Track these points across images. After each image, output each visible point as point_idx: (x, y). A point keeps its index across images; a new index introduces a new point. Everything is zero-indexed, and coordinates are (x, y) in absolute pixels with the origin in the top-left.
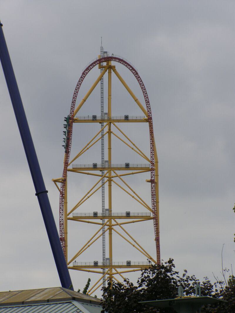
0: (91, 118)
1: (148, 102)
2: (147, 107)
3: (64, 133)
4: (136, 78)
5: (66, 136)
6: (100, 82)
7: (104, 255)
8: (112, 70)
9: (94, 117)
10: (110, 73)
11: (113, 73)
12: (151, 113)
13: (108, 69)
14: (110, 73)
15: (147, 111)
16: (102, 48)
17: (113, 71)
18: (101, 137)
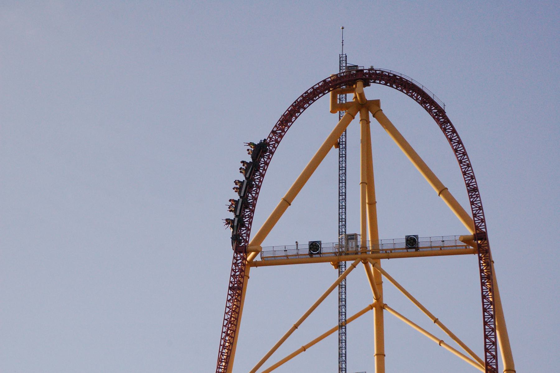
0: (305, 248)
1: (473, 190)
2: (472, 203)
3: (241, 165)
4: (468, 197)
5: (240, 194)
6: (334, 151)
7: (342, 221)
8: (369, 112)
9: (315, 247)
10: (366, 122)
11: (374, 122)
12: (483, 221)
13: (360, 110)
14: (366, 122)
15: (472, 216)
16: (343, 58)
17: (374, 116)
18: (337, 324)
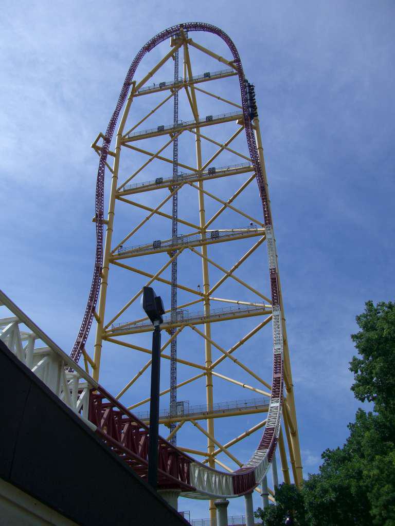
14: (186, 49)
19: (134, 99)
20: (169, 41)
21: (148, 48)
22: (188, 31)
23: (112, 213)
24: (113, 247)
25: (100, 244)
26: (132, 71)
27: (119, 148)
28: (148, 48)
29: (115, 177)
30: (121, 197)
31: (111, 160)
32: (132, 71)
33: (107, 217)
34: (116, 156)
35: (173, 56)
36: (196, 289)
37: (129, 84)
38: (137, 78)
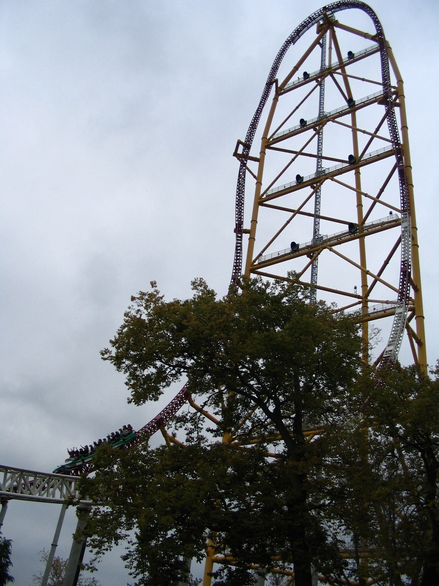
14: (333, 36)
19: (280, 98)
20: (314, 28)
21: (293, 40)
22: (333, 13)
23: (254, 221)
24: (255, 254)
25: (240, 242)
26: (275, 69)
27: (263, 153)
28: (293, 40)
29: (259, 184)
30: (271, 146)
31: (252, 165)
32: (275, 69)
33: (247, 225)
34: (260, 161)
35: (320, 44)
36: (352, 292)
37: (272, 84)
38: (281, 76)
